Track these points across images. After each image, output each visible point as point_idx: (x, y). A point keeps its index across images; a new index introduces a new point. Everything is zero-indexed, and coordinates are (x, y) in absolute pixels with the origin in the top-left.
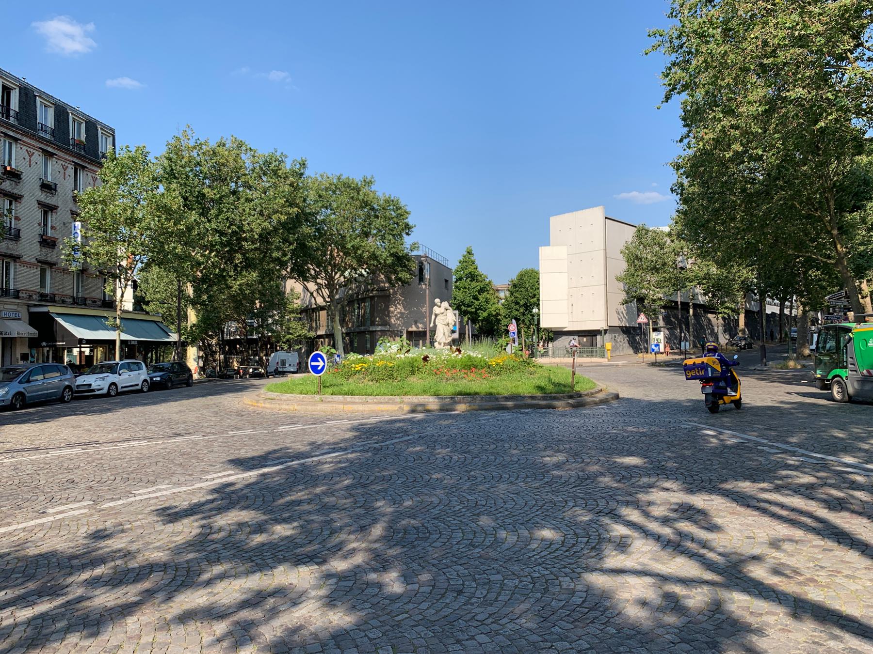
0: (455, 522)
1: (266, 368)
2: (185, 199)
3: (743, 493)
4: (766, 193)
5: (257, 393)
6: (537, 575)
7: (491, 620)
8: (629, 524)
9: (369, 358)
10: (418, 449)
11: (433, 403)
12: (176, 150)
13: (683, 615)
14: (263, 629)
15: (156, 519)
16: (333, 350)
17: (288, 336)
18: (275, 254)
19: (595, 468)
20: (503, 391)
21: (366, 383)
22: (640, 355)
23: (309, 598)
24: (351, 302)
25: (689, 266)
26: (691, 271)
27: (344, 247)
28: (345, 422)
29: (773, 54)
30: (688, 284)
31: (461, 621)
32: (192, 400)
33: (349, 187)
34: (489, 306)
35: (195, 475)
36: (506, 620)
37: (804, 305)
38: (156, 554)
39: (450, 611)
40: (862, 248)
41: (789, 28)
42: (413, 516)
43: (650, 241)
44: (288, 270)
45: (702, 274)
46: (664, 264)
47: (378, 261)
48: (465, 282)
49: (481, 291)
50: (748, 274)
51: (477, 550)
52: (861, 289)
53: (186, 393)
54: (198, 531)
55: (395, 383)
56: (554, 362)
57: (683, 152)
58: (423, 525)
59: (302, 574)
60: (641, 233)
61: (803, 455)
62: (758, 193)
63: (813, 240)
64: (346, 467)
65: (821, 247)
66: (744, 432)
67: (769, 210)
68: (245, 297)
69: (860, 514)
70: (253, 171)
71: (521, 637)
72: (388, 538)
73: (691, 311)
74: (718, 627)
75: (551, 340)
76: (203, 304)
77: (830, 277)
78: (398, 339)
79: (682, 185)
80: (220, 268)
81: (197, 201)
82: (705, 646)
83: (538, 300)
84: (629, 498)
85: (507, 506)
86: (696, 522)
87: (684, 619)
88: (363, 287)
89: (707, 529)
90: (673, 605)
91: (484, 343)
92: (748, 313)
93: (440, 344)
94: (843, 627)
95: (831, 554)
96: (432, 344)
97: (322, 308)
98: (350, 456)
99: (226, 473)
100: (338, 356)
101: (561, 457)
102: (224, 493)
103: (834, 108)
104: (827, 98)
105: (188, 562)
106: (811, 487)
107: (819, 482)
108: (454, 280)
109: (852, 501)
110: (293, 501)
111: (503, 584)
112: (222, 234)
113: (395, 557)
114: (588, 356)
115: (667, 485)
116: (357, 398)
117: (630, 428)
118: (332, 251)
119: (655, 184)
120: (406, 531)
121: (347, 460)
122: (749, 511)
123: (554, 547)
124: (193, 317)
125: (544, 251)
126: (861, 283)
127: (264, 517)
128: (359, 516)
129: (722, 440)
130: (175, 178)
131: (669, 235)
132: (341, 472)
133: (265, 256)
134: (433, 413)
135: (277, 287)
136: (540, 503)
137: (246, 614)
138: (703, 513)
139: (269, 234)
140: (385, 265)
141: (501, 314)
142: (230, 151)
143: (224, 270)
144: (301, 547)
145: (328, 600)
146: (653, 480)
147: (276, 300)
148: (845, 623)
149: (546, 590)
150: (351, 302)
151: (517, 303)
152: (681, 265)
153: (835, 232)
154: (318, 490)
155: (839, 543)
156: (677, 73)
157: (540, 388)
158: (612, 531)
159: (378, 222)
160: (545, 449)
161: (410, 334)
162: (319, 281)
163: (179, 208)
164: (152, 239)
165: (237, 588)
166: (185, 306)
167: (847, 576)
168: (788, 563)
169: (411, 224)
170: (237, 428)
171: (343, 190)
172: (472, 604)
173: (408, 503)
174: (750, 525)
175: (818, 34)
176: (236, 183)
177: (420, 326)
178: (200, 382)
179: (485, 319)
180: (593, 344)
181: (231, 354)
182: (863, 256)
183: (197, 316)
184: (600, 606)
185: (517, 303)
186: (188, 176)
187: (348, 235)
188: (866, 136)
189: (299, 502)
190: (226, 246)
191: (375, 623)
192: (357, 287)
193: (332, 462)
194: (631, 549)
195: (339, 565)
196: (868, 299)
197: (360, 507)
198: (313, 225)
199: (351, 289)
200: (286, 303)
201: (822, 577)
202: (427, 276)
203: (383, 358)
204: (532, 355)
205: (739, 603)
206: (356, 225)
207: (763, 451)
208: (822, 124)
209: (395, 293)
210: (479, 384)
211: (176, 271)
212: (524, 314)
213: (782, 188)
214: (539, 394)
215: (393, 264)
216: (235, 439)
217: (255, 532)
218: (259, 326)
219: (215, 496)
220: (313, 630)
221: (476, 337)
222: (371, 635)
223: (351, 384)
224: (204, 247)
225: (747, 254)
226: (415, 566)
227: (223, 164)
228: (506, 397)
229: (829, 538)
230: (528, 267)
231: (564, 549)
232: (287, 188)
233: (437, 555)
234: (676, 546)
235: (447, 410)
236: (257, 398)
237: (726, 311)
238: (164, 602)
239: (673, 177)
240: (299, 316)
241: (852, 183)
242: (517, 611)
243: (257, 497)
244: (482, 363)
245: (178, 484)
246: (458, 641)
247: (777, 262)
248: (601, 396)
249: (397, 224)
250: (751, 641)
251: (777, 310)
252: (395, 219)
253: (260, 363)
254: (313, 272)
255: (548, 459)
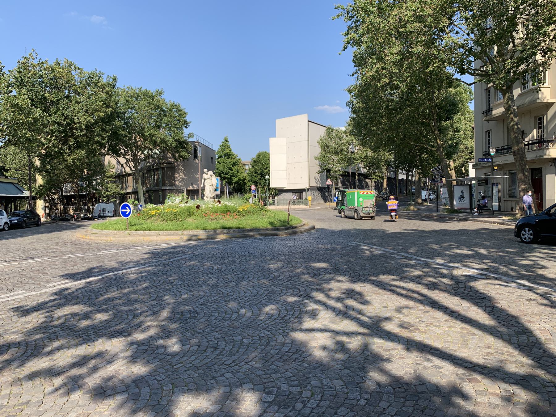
0: (214, 306)
1: (92, 214)
2: (32, 100)
3: (382, 282)
4: (399, 109)
5: (85, 230)
6: (263, 335)
7: (234, 364)
8: (318, 302)
9: (161, 207)
10: (192, 263)
11: (202, 234)
12: (24, 67)
13: (347, 353)
14: (87, 380)
15: (12, 314)
16: (136, 202)
17: (107, 193)
18: (97, 139)
19: (300, 270)
20: (247, 226)
21: (159, 223)
22: (328, 203)
23: (118, 358)
24: (149, 171)
25: (356, 151)
26: (357, 154)
27: (143, 135)
28: (145, 247)
29: (405, 26)
30: (355, 162)
31: (215, 366)
32: (40, 235)
33: (147, 96)
34: (239, 174)
35: (42, 284)
36: (243, 363)
37: (419, 174)
38: (12, 337)
39: (209, 360)
40: (451, 142)
41: (414, 11)
42: (188, 304)
43: (334, 136)
44: (106, 149)
45: (363, 156)
46: (342, 150)
47: (167, 144)
48: (224, 159)
49: (234, 165)
50: (389, 156)
51: (227, 322)
52: (450, 165)
53: (37, 231)
54: (43, 320)
55: (178, 222)
56: (278, 209)
57: (353, 82)
58: (194, 309)
59: (114, 344)
60: (329, 131)
61: (415, 259)
62: (395, 109)
63: (424, 137)
64: (144, 276)
65: (429, 140)
66: (384, 247)
67: (400, 119)
68: (77, 167)
69: (444, 291)
70: (80, 83)
71: (252, 373)
72: (171, 319)
73: (357, 177)
74: (366, 359)
75: (277, 195)
76: (47, 171)
77: (434, 157)
78: (180, 194)
79: (353, 102)
80: (58, 148)
81: (45, 105)
82: (358, 370)
83: (269, 171)
84: (318, 287)
85: (247, 295)
86: (356, 300)
87: (347, 356)
88: (157, 161)
89: (361, 303)
90: (341, 348)
91: (236, 197)
92: (389, 179)
93: (207, 197)
94: (432, 354)
95: (428, 314)
96: (203, 196)
97: (130, 175)
98: (147, 269)
99: (63, 282)
100: (141, 206)
101: (280, 265)
102: (62, 295)
103: (437, 60)
104: (433, 54)
105: (35, 340)
106: (419, 277)
107: (424, 274)
108: (217, 158)
109: (440, 284)
110: (109, 298)
111: (242, 341)
112: (59, 124)
113: (175, 330)
114: (298, 205)
115: (340, 278)
116: (152, 232)
117: (321, 246)
118: (135, 137)
119: (338, 101)
120: (182, 313)
121: (146, 272)
122: (385, 292)
123: (273, 318)
124: (40, 180)
125: (272, 141)
126: (450, 162)
127: (89, 309)
128: (152, 306)
129: (371, 252)
130: (25, 85)
131: (345, 132)
132: (142, 279)
133: (90, 140)
134: (203, 241)
135: (99, 160)
136: (266, 292)
137: (75, 372)
138: (360, 294)
139: (92, 125)
140: (171, 147)
141: (246, 180)
142: (63, 69)
143: (61, 149)
144: (114, 326)
145: (131, 358)
146: (332, 276)
147: (99, 169)
148: (433, 351)
149: (268, 344)
150: (149, 171)
151: (256, 172)
152: (351, 150)
153: (436, 132)
154: (126, 291)
155: (432, 307)
156: (353, 34)
157: (272, 223)
158: (307, 307)
159: (166, 119)
160: (271, 260)
161: (189, 192)
162: (127, 157)
163: (28, 106)
164: (8, 127)
165: (70, 355)
166: (34, 172)
167: (435, 326)
168: (405, 320)
169: (188, 121)
170: (71, 253)
171: (143, 97)
172: (223, 355)
173: (185, 296)
174: (385, 300)
175: (429, 15)
176: (69, 90)
177: (195, 186)
178: (46, 223)
179: (236, 182)
180: (301, 197)
181: (68, 204)
182: (451, 146)
183: (43, 179)
184: (299, 351)
185: (256, 172)
186: (33, 85)
187: (146, 127)
188: (454, 77)
189: (113, 299)
190: (62, 133)
191: (161, 370)
192: (153, 161)
193: (135, 273)
194: (318, 317)
195: (139, 336)
196: (453, 171)
197: (153, 300)
198: (122, 120)
199: (148, 162)
200: (105, 171)
201: (422, 327)
202: (199, 155)
203: (170, 207)
204: (265, 204)
205: (378, 345)
206: (152, 121)
207: (394, 257)
208: (430, 69)
209: (178, 165)
210: (232, 222)
211: (26, 149)
212: (260, 179)
213: (408, 106)
214: (269, 227)
215: (177, 146)
216: (70, 260)
217: (83, 319)
218: (87, 186)
219: (56, 297)
220: (121, 378)
221: (231, 193)
222: (158, 378)
223: (149, 223)
224: (47, 134)
225: (389, 143)
226: (188, 334)
227: (58, 78)
228: (248, 230)
229: (427, 305)
230: (263, 150)
231: (280, 318)
232: (104, 95)
233: (202, 327)
234: (344, 314)
235: (212, 239)
236: (86, 233)
237: (376, 177)
238: (18, 367)
239: (348, 97)
240: (114, 180)
241: (446, 105)
242: (250, 357)
243: (84, 296)
244: (234, 210)
245: (30, 290)
246: (214, 378)
247: (405, 149)
248: (306, 227)
249: (179, 120)
250: (383, 365)
251: (404, 177)
252: (177, 117)
253: (88, 210)
254: (123, 151)
255: (272, 265)
